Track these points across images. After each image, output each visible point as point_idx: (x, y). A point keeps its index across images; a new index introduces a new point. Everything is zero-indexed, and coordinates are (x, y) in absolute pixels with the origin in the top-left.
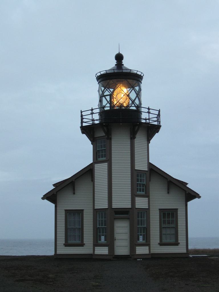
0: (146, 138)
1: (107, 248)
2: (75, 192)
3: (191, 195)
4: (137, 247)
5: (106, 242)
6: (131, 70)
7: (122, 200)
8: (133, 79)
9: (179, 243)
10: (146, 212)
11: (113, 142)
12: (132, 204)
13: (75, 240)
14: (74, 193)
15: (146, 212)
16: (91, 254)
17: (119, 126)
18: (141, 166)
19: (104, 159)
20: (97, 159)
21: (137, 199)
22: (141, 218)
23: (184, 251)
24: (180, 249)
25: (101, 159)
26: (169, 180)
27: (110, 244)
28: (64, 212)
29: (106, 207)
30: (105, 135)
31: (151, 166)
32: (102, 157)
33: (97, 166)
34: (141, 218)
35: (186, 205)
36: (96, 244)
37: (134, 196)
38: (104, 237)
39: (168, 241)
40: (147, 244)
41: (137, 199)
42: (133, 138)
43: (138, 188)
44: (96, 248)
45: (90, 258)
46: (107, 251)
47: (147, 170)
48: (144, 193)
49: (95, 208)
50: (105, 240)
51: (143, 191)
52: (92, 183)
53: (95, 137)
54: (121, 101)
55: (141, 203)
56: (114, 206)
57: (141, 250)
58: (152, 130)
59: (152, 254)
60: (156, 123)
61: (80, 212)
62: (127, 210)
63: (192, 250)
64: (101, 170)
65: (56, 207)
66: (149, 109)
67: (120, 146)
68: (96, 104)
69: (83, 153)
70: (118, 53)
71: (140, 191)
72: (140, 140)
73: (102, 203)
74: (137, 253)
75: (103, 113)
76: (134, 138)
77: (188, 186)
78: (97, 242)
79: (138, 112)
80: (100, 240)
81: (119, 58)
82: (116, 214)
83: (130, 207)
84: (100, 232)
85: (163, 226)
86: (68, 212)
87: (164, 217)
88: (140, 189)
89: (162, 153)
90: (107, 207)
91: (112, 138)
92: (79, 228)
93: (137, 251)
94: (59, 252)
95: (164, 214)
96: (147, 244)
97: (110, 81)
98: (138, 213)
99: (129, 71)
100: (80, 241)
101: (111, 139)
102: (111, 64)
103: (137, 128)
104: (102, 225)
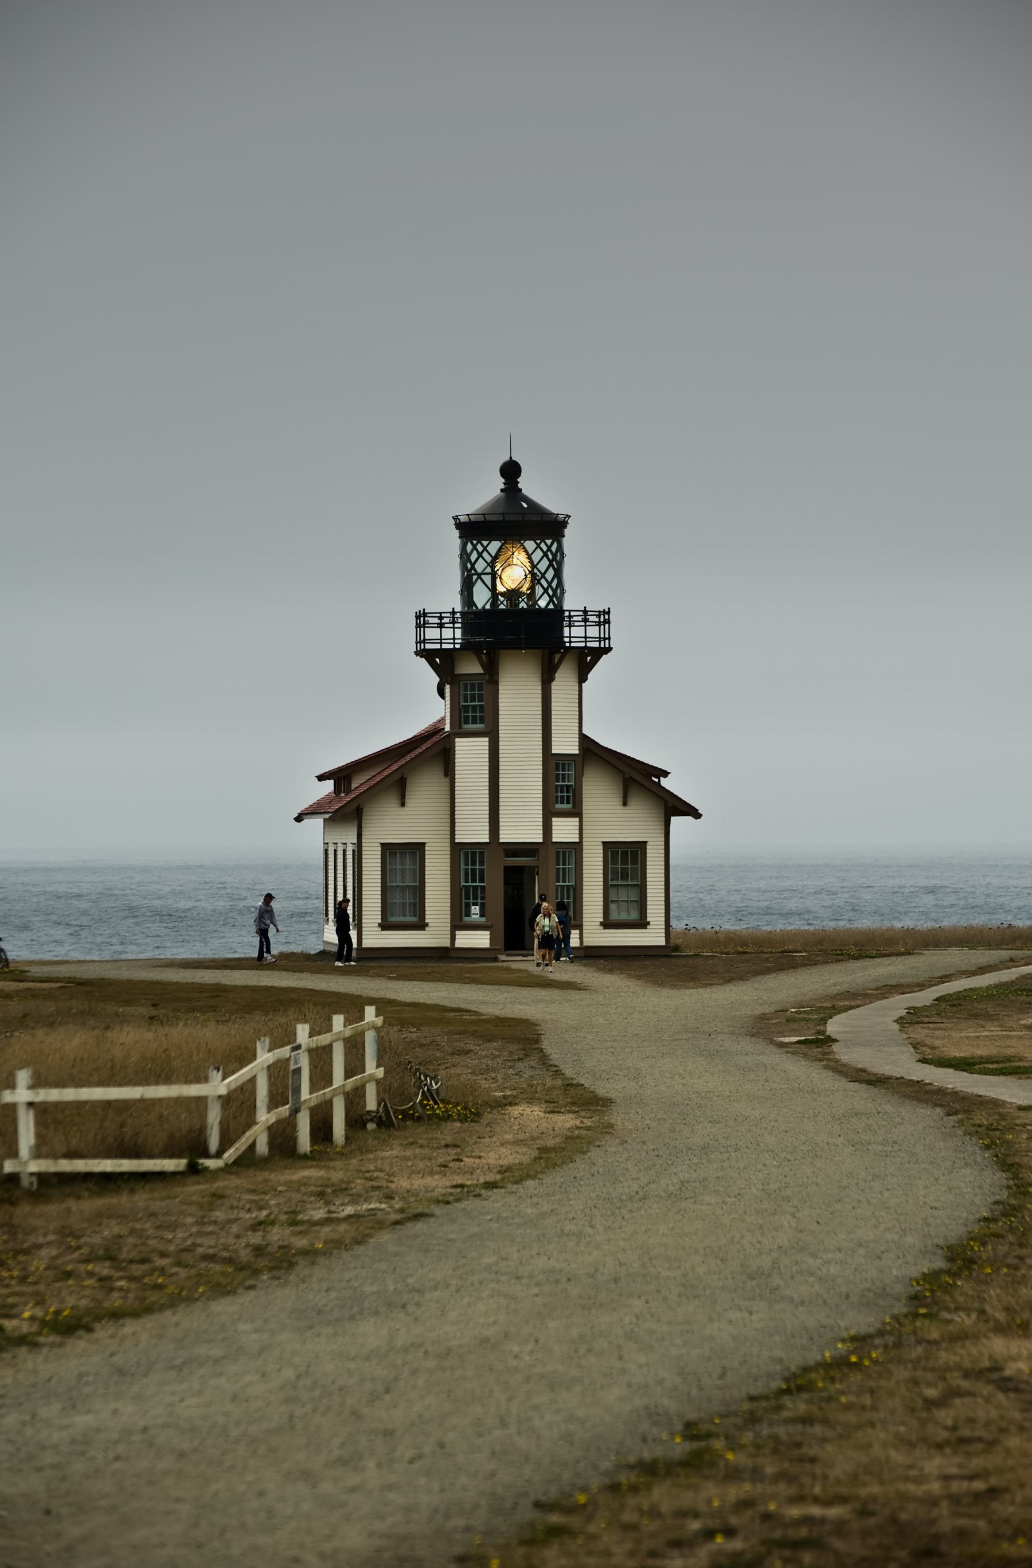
0: (577, 676)
1: (488, 933)
3: (676, 807)
4: (457, 740)
5: (483, 919)
7: (522, 826)
8: (549, 528)
9: (649, 923)
10: (575, 849)
11: (501, 688)
12: (544, 834)
13: (405, 916)
14: (403, 805)
15: (575, 849)
16: (445, 948)
17: (505, 642)
18: (565, 744)
19: (479, 726)
20: (460, 727)
22: (564, 864)
23: (662, 942)
24: (653, 936)
25: (471, 727)
26: (627, 776)
29: (485, 838)
31: (585, 742)
32: (474, 722)
33: (462, 744)
34: (564, 864)
36: (458, 922)
37: (548, 815)
39: (624, 916)
44: (457, 932)
46: (488, 941)
47: (577, 752)
48: (570, 806)
49: (457, 841)
50: (482, 915)
51: (568, 803)
52: (447, 780)
53: (457, 672)
55: (564, 830)
56: (504, 838)
58: (587, 659)
59: (588, 947)
61: (417, 850)
64: (471, 753)
65: (359, 836)
66: (585, 612)
67: (517, 694)
68: (456, 603)
69: (422, 705)
72: (563, 683)
73: (473, 830)
75: (473, 620)
76: (552, 679)
77: (664, 782)
78: (461, 920)
79: (556, 617)
80: (468, 914)
81: (511, 471)
83: (541, 841)
84: (467, 898)
86: (388, 850)
87: (614, 862)
88: (562, 797)
89: (609, 710)
91: (500, 680)
95: (614, 855)
98: (558, 853)
100: (415, 916)
101: (497, 683)
102: (485, 492)
103: (557, 657)
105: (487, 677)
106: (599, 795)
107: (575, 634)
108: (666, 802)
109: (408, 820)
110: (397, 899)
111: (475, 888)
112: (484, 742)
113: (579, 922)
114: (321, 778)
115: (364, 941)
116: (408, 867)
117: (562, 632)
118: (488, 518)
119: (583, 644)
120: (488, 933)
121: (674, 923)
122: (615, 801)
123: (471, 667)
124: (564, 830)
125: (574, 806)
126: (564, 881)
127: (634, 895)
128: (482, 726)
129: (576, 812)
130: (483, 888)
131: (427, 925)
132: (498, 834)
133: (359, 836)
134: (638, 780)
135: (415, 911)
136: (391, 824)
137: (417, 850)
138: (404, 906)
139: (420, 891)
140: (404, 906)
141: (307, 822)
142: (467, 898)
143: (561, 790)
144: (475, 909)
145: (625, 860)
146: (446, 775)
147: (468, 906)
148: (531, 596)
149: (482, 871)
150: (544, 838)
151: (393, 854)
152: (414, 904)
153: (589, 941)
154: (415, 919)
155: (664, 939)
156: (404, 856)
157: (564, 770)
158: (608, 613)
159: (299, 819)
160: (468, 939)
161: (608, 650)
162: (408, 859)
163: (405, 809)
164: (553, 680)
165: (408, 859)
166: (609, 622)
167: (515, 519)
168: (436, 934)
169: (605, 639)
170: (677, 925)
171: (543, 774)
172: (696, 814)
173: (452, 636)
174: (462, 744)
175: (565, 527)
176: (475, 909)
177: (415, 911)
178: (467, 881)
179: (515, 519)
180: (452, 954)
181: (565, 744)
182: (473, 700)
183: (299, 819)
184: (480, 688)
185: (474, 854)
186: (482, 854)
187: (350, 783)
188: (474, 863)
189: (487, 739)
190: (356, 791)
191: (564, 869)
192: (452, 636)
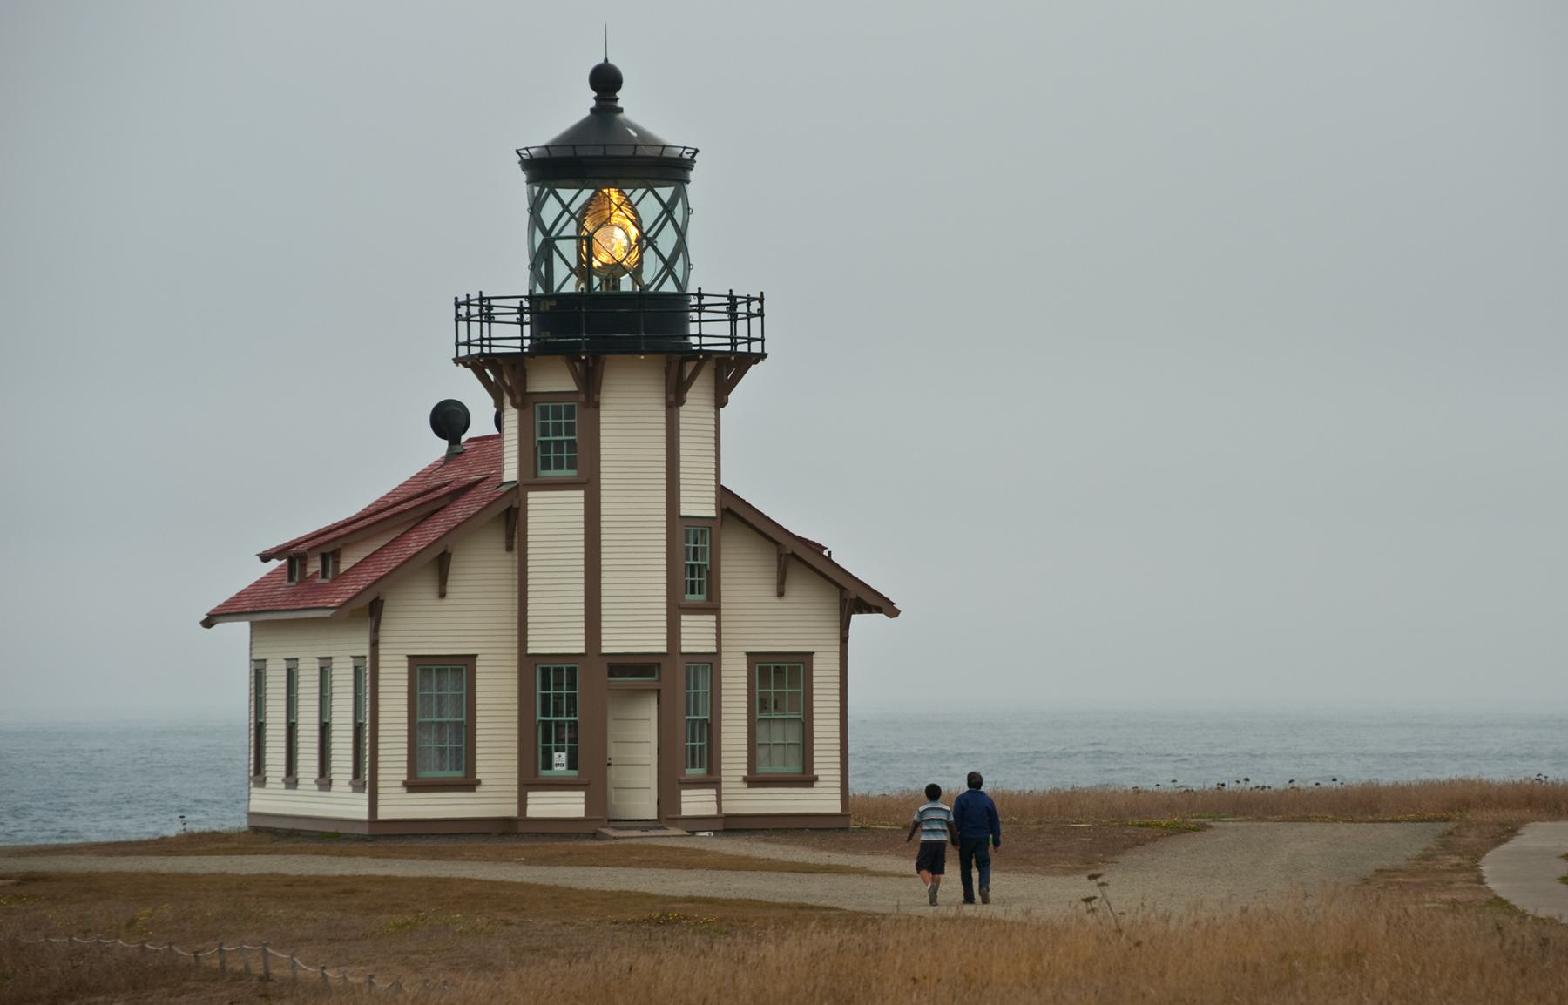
1: (582, 794)
2: (448, 590)
3: (856, 599)
4: (530, 494)
5: (574, 773)
6: (664, 146)
7: (636, 627)
8: (668, 169)
9: (816, 779)
10: (711, 662)
13: (441, 768)
14: (442, 595)
15: (711, 662)
17: (602, 339)
19: (565, 473)
21: (687, 621)
22: (696, 687)
23: (834, 807)
24: (822, 799)
25: (553, 473)
27: (592, 775)
28: (406, 664)
29: (575, 644)
30: (574, 388)
31: (723, 493)
32: (559, 466)
33: (538, 502)
35: (844, 640)
36: (530, 780)
37: (676, 611)
38: (564, 755)
39: (778, 769)
40: (712, 781)
41: (687, 621)
42: (674, 401)
43: (693, 583)
44: (530, 794)
45: (507, 832)
46: (583, 807)
49: (530, 651)
50: (572, 764)
53: (529, 390)
54: (620, 255)
55: (697, 634)
56: (611, 644)
57: (696, 803)
58: (731, 367)
60: (669, 287)
61: (466, 664)
62: (657, 660)
63: (865, 798)
64: (553, 516)
65: (375, 644)
66: (731, 298)
67: (628, 419)
70: (601, 61)
71: (693, 592)
73: (558, 634)
74: (684, 813)
76: (680, 401)
78: (536, 774)
80: (548, 765)
81: (606, 81)
82: (611, 674)
83: (664, 650)
85: (758, 716)
86: (420, 666)
89: (760, 447)
90: (582, 651)
91: (602, 401)
92: (459, 724)
93: (683, 806)
94: (384, 813)
95: (764, 673)
96: (712, 781)
97: (598, 190)
99: (655, 152)
100: (458, 769)
101: (597, 406)
104: (558, 713)
105: (582, 397)
106: (743, 575)
107: (710, 332)
108: (842, 589)
109: (456, 619)
110: (429, 742)
111: (559, 725)
112: (576, 498)
113: (715, 777)
114: (265, 557)
115: (529, 808)
116: (449, 692)
117: (686, 328)
118: (555, 153)
119: (728, 348)
120: (582, 794)
121: (852, 782)
122: (767, 588)
123: (555, 381)
124: (697, 634)
125: (709, 598)
126: (696, 713)
127: (793, 734)
128: (573, 473)
129: (712, 607)
130: (574, 726)
131: (479, 782)
132: (600, 640)
133: (375, 644)
134: (798, 560)
135: (458, 761)
136: (423, 626)
137: (466, 664)
138: (445, 752)
139: (466, 730)
140: (445, 752)
141: (221, 628)
142: (547, 739)
143: (693, 582)
144: (560, 758)
145: (780, 678)
146: (509, 548)
147: (548, 754)
148: (636, 273)
149: (572, 698)
150: (668, 646)
151: (427, 672)
152: (458, 750)
153: (730, 807)
154: (459, 774)
155: (838, 803)
156: (444, 677)
157: (695, 558)
158: (761, 300)
159: (208, 622)
160: (543, 805)
161: (762, 356)
162: (449, 679)
163: (445, 602)
164: (683, 402)
165: (449, 679)
166: (761, 313)
167: (600, 156)
168: (494, 798)
169: (750, 340)
170: (857, 786)
171: (668, 547)
172: (884, 606)
173: (510, 335)
174: (538, 502)
175: (691, 168)
176: (560, 758)
177: (458, 761)
178: (545, 713)
179: (600, 156)
180: (522, 828)
181: (699, 503)
182: (557, 432)
183: (208, 622)
184: (570, 413)
185: (558, 671)
186: (572, 672)
187: (337, 563)
188: (693, 740)
189: (581, 493)
190: (325, 580)
191: (696, 695)
192: (510, 335)
